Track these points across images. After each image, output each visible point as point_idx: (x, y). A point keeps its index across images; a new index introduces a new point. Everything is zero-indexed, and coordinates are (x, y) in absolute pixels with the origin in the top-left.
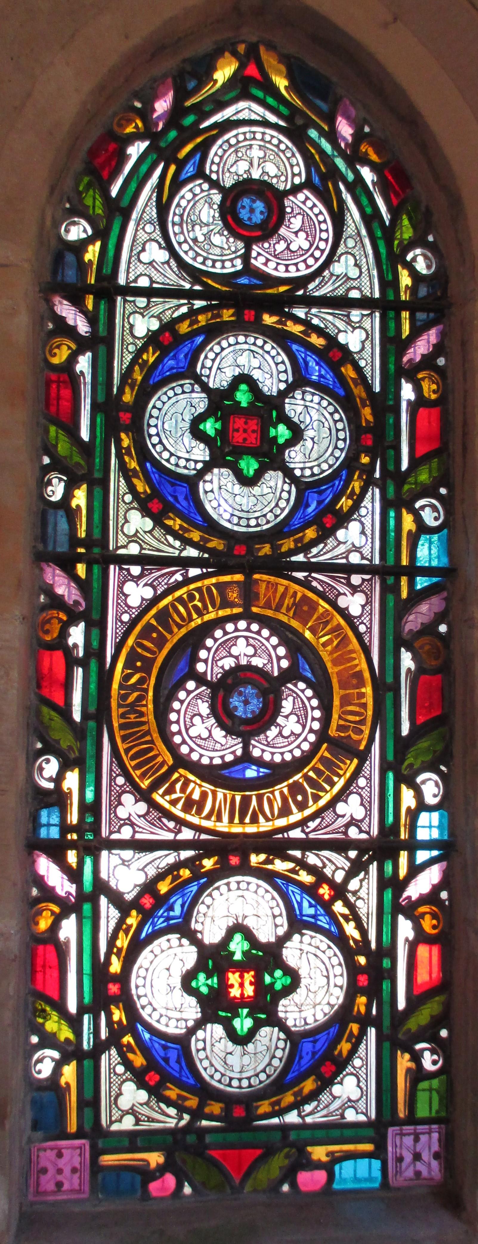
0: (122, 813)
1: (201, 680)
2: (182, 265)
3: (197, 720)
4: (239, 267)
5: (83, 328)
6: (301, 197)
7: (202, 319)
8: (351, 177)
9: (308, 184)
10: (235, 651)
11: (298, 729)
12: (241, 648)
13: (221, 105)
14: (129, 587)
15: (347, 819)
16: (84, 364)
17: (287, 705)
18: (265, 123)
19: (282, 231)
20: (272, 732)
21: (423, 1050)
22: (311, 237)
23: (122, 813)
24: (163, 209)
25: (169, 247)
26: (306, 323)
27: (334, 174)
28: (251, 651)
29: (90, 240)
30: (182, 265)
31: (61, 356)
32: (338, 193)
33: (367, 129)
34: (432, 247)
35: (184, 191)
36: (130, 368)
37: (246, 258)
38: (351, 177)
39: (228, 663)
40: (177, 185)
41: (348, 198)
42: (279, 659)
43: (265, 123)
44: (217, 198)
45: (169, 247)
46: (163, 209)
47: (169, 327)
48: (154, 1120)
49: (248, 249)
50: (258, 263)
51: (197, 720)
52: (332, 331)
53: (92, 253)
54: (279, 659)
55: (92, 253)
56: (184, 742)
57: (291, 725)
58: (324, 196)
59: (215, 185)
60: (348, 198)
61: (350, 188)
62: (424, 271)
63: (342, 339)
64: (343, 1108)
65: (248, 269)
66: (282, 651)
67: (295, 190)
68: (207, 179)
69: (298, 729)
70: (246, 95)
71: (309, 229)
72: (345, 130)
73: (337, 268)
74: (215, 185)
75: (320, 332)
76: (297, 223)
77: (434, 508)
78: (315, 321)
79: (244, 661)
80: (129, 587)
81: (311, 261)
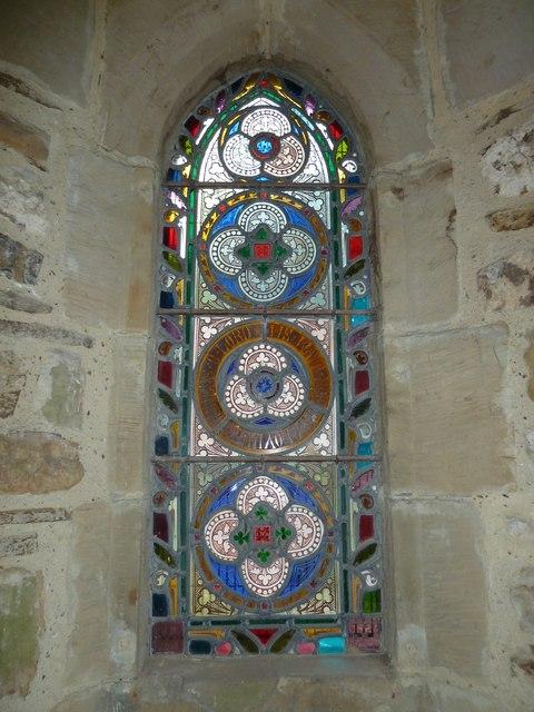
0: (201, 444)
1: (241, 374)
2: (230, 173)
3: (239, 395)
4: (258, 172)
5: (180, 204)
6: (289, 139)
7: (242, 198)
8: (312, 128)
9: (292, 133)
10: (258, 360)
11: (292, 399)
12: (262, 358)
13: (249, 100)
14: (204, 329)
15: (320, 447)
16: (183, 222)
17: (286, 387)
18: (271, 107)
19: (280, 155)
20: (279, 401)
21: (366, 575)
22: (294, 157)
23: (201, 444)
24: (221, 149)
25: (224, 166)
26: (292, 198)
27: (304, 128)
28: (266, 359)
29: (186, 164)
30: (230, 173)
31: (172, 218)
32: (307, 137)
33: (361, 213)
34: (356, 160)
35: (231, 140)
36: (205, 223)
37: (262, 169)
38: (312, 128)
39: (255, 366)
40: (228, 137)
41: (311, 138)
42: (281, 363)
43: (271, 107)
44: (278, 134)
45: (224, 166)
46: (221, 149)
47: (224, 202)
48: (219, 611)
49: (263, 164)
50: (268, 171)
51: (239, 395)
52: (305, 201)
53: (187, 171)
54: (281, 363)
55: (187, 171)
56: (233, 407)
57: (289, 397)
58: (300, 138)
59: (246, 136)
60: (311, 138)
61: (313, 133)
62: (352, 171)
63: (311, 204)
64: (320, 451)
65: (263, 174)
66: (283, 359)
67: (286, 136)
68: (243, 134)
69: (292, 399)
70: (260, 95)
71: (293, 153)
72: (310, 111)
73: (306, 171)
74: (246, 136)
75: (300, 201)
76: (287, 151)
77: (361, 286)
78: (297, 197)
79: (263, 365)
80: (204, 329)
81: (294, 169)
